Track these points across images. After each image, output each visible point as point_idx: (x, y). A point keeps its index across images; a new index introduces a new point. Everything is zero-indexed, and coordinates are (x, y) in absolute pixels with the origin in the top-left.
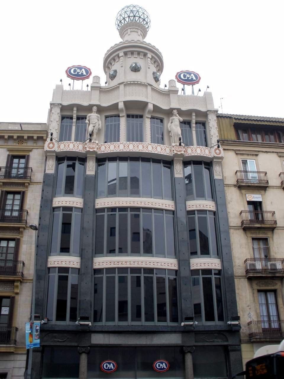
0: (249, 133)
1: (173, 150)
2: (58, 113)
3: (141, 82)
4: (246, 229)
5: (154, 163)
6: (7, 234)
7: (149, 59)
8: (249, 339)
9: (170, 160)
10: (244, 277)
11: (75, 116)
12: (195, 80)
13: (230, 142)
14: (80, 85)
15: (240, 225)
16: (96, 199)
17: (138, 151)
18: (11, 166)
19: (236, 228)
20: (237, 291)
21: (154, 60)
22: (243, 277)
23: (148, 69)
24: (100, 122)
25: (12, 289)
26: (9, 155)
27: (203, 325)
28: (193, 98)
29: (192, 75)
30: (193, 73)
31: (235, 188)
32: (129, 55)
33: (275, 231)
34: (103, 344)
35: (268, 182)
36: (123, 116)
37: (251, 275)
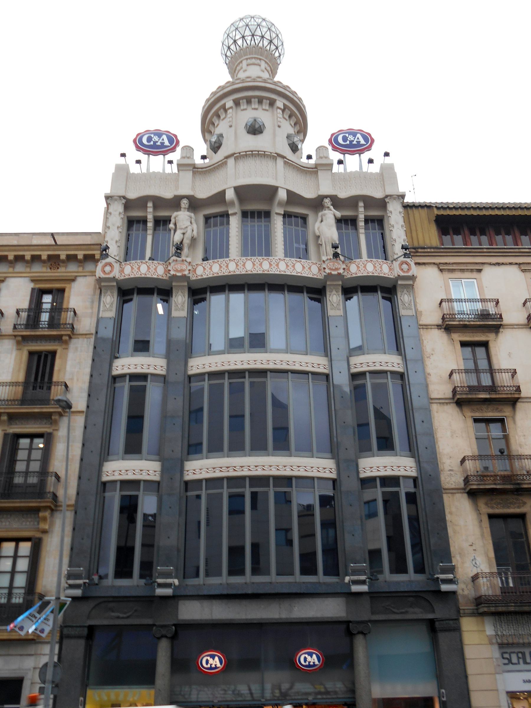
0: (464, 234)
1: (324, 268)
2: (120, 213)
3: (265, 152)
4: (461, 401)
5: (290, 293)
6: (28, 426)
7: (280, 111)
8: (476, 608)
9: (319, 286)
10: (462, 491)
11: (150, 217)
12: (364, 145)
13: (429, 250)
14: (157, 164)
15: (450, 395)
16: (189, 360)
17: (278, 273)
18: (37, 307)
19: (443, 402)
20: (448, 517)
21: (288, 112)
22: (459, 491)
23: (277, 128)
24: (195, 226)
25: (36, 523)
26: (33, 289)
27: (386, 581)
28: (361, 176)
29: (358, 135)
30: (359, 133)
31: (440, 331)
33: (519, 405)
34: (201, 620)
35: (501, 317)
36: (235, 214)
37: (475, 487)
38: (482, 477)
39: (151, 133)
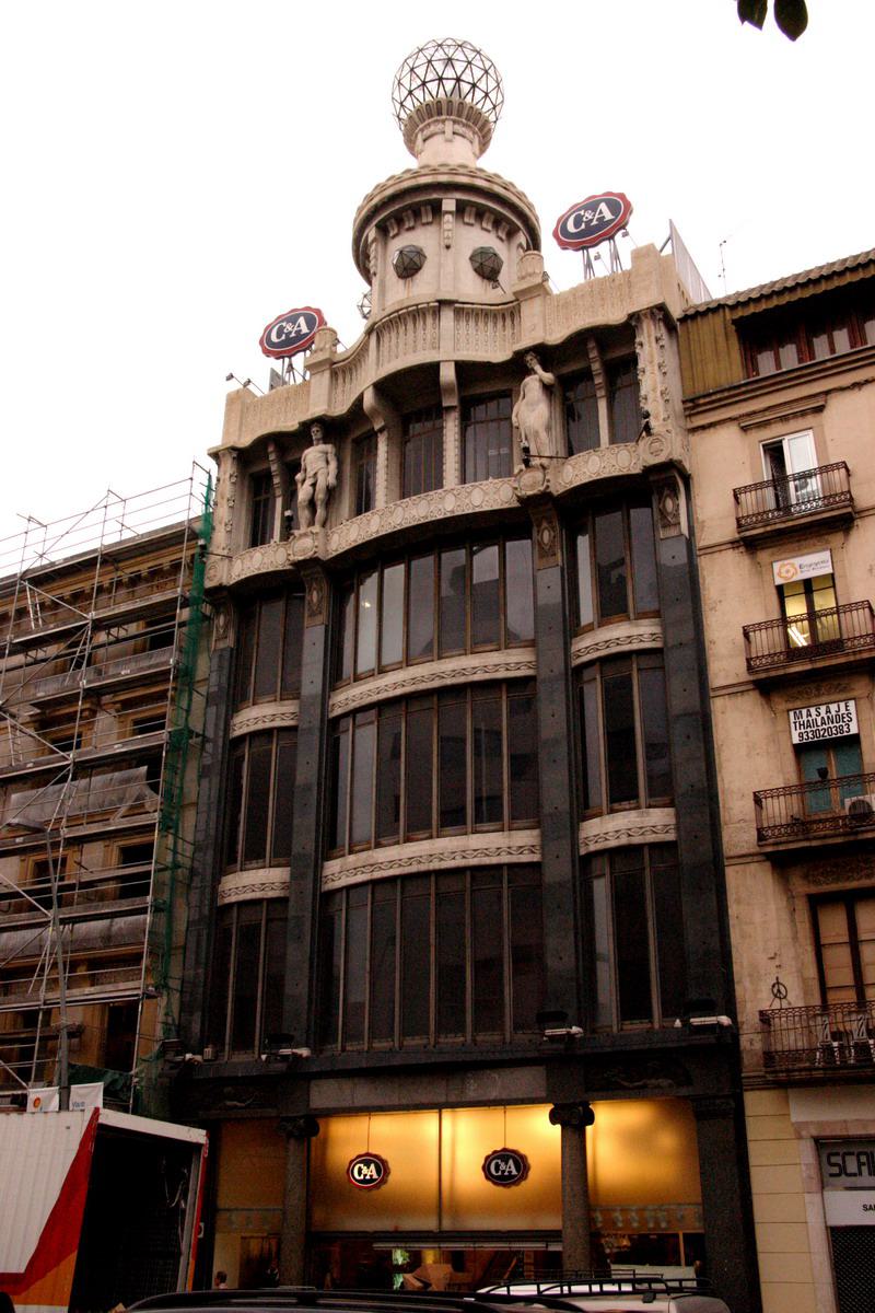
3: (417, 305)
13: (719, 396)
19: (733, 690)
22: (756, 859)
23: (444, 251)
32: (409, 220)
38: (800, 825)
39: (580, 210)
